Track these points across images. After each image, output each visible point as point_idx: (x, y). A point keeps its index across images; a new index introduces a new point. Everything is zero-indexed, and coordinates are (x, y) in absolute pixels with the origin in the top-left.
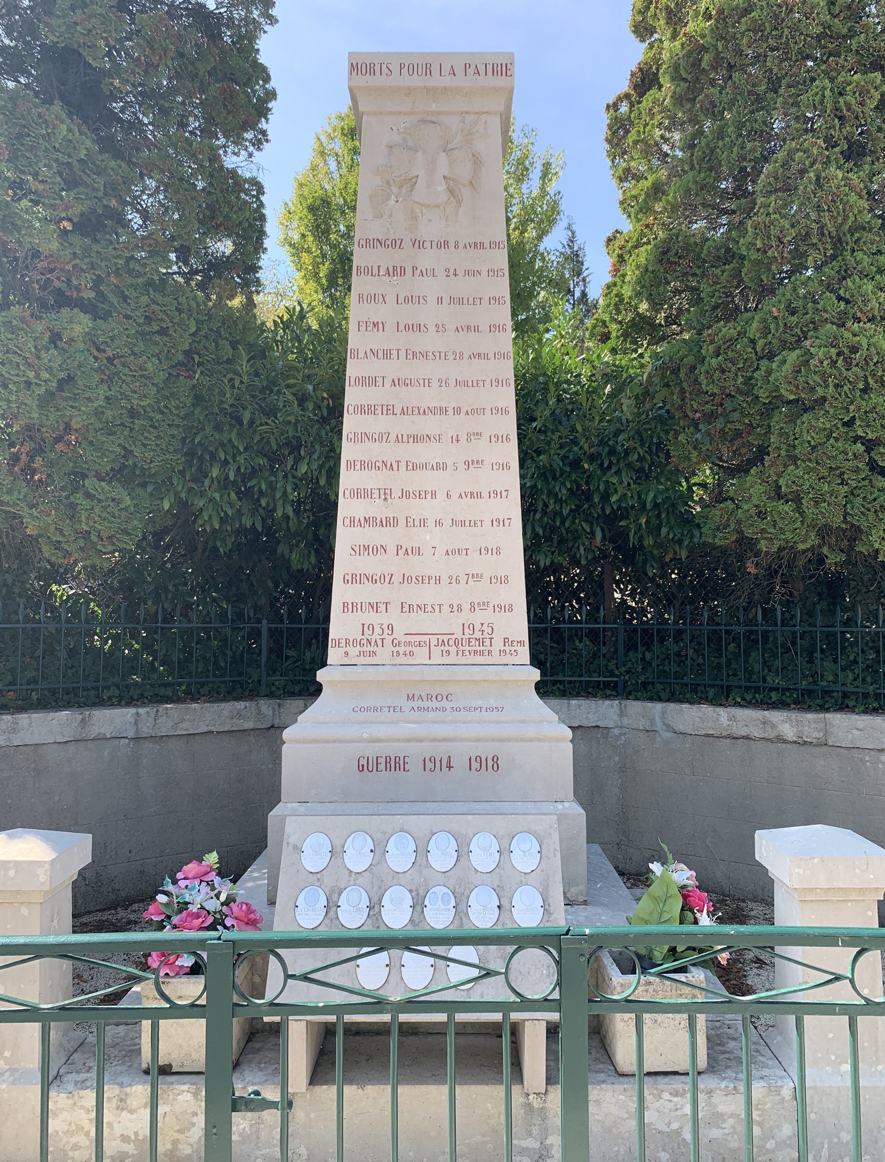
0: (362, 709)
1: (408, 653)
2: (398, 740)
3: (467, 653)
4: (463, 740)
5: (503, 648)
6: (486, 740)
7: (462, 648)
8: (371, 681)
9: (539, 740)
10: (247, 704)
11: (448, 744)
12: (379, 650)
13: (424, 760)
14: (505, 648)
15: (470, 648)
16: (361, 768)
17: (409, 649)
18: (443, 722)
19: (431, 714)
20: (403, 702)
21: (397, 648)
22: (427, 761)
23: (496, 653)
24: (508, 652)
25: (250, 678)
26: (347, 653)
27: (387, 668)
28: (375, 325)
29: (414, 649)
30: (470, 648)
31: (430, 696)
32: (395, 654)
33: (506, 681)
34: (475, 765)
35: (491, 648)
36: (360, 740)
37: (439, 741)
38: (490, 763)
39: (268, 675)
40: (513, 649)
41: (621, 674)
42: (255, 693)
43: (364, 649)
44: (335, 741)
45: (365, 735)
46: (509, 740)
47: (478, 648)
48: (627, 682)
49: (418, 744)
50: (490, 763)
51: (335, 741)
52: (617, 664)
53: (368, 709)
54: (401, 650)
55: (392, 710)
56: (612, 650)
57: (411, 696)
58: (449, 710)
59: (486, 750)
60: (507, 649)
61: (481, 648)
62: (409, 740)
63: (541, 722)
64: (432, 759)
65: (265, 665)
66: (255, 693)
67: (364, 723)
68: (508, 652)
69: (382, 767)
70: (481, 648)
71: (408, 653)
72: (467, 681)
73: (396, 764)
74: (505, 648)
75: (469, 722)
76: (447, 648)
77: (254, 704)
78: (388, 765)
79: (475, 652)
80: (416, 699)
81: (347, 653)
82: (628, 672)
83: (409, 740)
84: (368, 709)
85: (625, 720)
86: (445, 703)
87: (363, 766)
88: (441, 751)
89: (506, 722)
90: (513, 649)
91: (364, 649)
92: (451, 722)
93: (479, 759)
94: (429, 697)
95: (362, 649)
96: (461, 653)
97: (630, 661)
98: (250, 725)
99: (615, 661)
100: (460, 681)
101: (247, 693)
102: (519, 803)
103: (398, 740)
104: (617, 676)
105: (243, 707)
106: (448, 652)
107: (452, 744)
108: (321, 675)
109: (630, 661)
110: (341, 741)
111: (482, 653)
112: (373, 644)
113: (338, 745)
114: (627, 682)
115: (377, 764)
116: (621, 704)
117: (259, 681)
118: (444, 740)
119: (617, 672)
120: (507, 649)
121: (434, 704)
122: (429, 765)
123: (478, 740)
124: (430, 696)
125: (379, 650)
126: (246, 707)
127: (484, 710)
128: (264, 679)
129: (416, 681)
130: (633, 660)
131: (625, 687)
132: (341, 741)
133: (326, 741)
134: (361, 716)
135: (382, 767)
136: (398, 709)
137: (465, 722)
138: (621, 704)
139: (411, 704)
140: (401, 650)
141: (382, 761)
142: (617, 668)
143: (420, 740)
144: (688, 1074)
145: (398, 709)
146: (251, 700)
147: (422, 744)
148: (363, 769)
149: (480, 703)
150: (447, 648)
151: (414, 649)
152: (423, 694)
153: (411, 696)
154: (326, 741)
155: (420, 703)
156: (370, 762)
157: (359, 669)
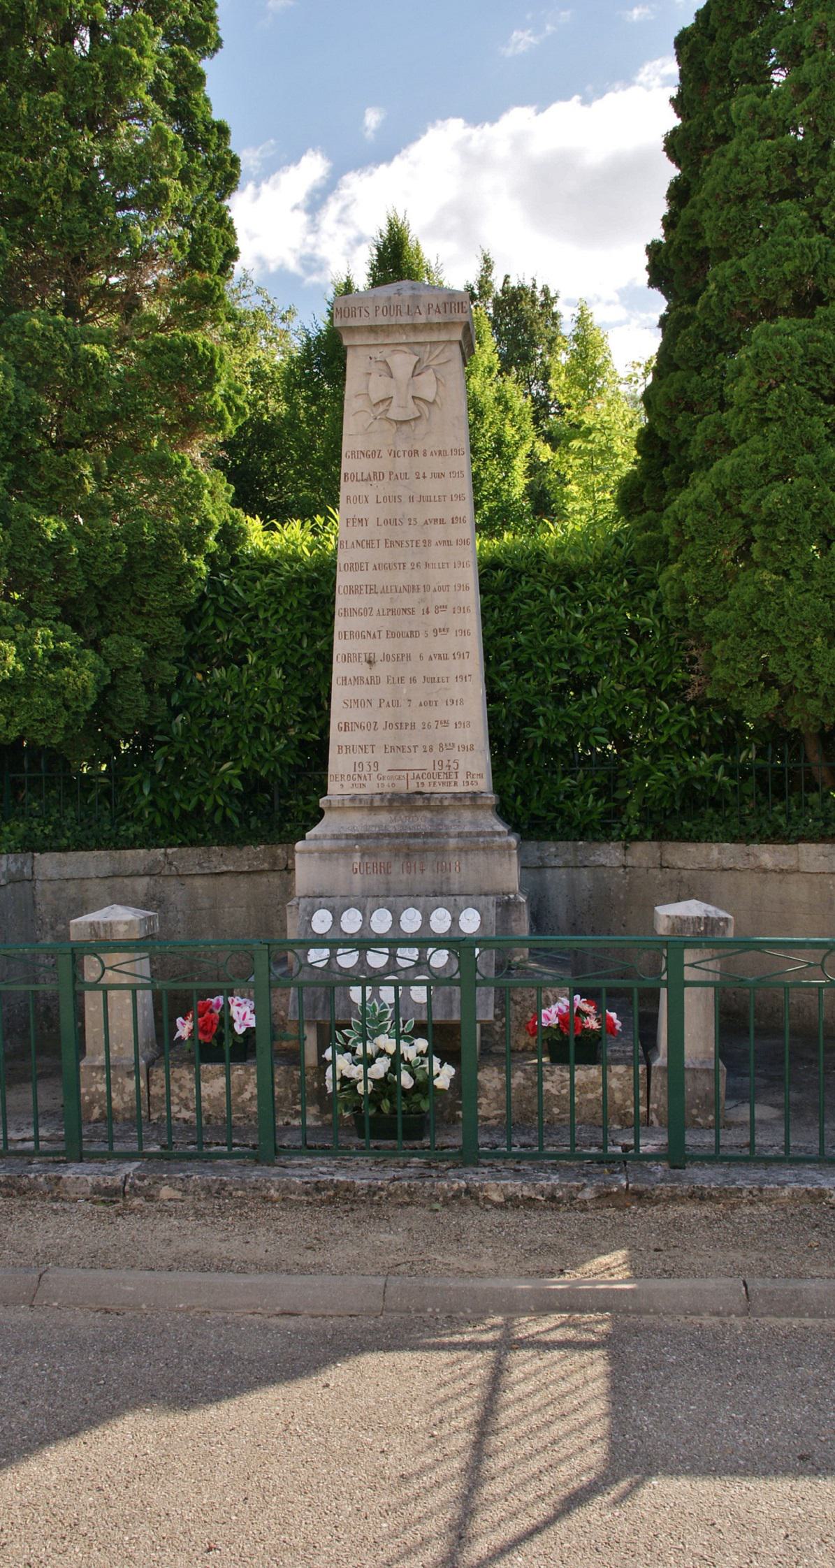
12: (367, 783)
28: (361, 521)
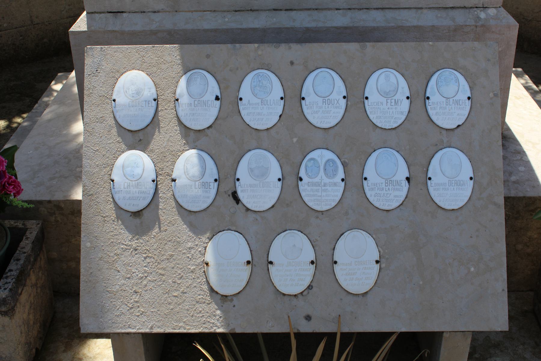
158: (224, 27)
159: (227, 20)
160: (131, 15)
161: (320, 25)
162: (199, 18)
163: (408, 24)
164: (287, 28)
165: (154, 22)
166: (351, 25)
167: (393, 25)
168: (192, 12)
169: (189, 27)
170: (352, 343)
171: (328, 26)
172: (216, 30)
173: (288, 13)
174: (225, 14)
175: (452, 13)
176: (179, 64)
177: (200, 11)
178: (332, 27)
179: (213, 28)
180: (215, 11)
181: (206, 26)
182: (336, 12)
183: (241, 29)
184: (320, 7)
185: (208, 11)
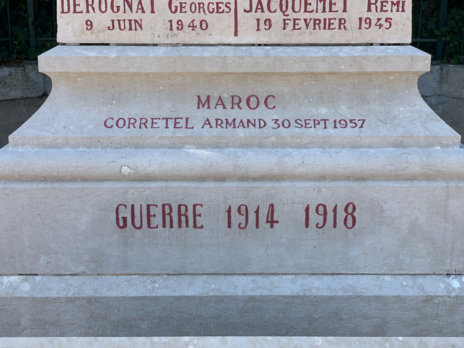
0: (121, 123)
1: (197, 23)
2: (184, 179)
3: (302, 24)
4: (294, 178)
5: (365, 15)
6: (335, 178)
7: (293, 16)
8: (134, 74)
9: (427, 178)
10: (12, 70)
11: (269, 185)
12: (146, 18)
13: (229, 211)
14: (369, 15)
15: (308, 16)
16: (122, 224)
17: (198, 17)
18: (261, 146)
19: (241, 132)
20: (189, 109)
21: (178, 16)
22: (234, 211)
23: (352, 23)
24: (374, 22)
25: (16, 40)
26: (89, 24)
27: (160, 51)
29: (209, 17)
30: (308, 16)
31: (236, 100)
32: (175, 25)
33: (370, 74)
34: (315, 218)
35: (345, 15)
36: (119, 178)
37: (255, 179)
38: (341, 215)
39: (37, 35)
40: (384, 16)
41: (443, 35)
42: (24, 56)
43: (120, 15)
44: (74, 179)
45: (126, 170)
46: (373, 177)
47: (321, 16)
48: (448, 43)
49: (218, 184)
50: (341, 215)
51: (74, 179)
52: (437, 22)
53: (130, 123)
54: (186, 18)
55: (171, 124)
56: (432, 6)
57: (203, 100)
58: (271, 124)
59: (334, 195)
60: (374, 16)
61: (328, 15)
62: (202, 178)
63: (432, 145)
64: (243, 210)
65: (33, 24)
66: (24, 56)
67: (125, 146)
68: (374, 22)
69: (157, 220)
70: (328, 15)
71: (197, 23)
72: (301, 74)
73: (181, 216)
74: (369, 15)
75: (306, 146)
76: (267, 15)
77: (20, 70)
78: (168, 218)
79: (316, 22)
80: (212, 105)
81: (89, 24)
82: (449, 32)
83: (202, 178)
84: (130, 123)
85: (445, 88)
86: (262, 112)
87: (125, 219)
88: (259, 194)
89: (370, 147)
90: (384, 16)
91: (120, 15)
92: (275, 146)
93: (322, 209)
94: (236, 102)
95: (116, 17)
96: (291, 23)
97: (453, 19)
98: (17, 94)
99: (435, 20)
100: (289, 74)
101: (14, 56)
102: (387, 278)
103: (184, 179)
104: (436, 36)
105: (7, 74)
106: (268, 22)
107: (277, 185)
108: (47, 62)
109: (453, 19)
110: (84, 179)
111: (328, 24)
112: (135, 7)
113: (78, 185)
114: (448, 43)
115: (149, 216)
116: (442, 69)
117: (28, 42)
118: (263, 178)
119: (437, 32)
120: (374, 16)
121: (244, 114)
122: (237, 218)
123: (322, 178)
124: (236, 100)
125: (146, 18)
126: (10, 74)
127: (330, 124)
128: (32, 39)
129: (213, 74)
130: (457, 18)
131: (444, 49)
132: (84, 179)
133: (60, 179)
134: (120, 134)
135: (157, 220)
136: (182, 123)
137: (299, 146)
138: (442, 69)
139: (205, 113)
140: (186, 18)
141: (157, 211)
142: (438, 27)
143: (221, 178)
144: (236, 35)
145: (182, 123)
146: (18, 65)
147: (226, 185)
148: (125, 225)
149: (323, 112)
150: (267, 15)
151: (209, 17)
152: (225, 96)
153: (203, 100)
154: (60, 179)
155: (219, 112)
156: (137, 213)
157: (112, 52)
158: (154, 295)
159: (157, 285)
160: (45, 279)
161: (265, 293)
162: (126, 283)
163: (369, 294)
164: (229, 297)
165: (72, 288)
166: (301, 294)
167: (351, 294)
168: (117, 275)
169: (113, 294)
170: (31, 20)
171: (274, 294)
172: (144, 298)
173: (229, 277)
174: (156, 278)
175: (420, 280)
176: (244, 292)
177: (127, 275)
178: (279, 296)
179: (141, 295)
180: (143, 274)
181: (133, 294)
182: (284, 277)
183: (173, 297)
184: (265, 272)
185: (137, 274)
